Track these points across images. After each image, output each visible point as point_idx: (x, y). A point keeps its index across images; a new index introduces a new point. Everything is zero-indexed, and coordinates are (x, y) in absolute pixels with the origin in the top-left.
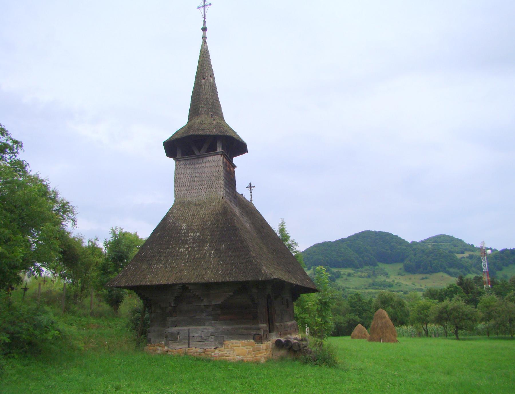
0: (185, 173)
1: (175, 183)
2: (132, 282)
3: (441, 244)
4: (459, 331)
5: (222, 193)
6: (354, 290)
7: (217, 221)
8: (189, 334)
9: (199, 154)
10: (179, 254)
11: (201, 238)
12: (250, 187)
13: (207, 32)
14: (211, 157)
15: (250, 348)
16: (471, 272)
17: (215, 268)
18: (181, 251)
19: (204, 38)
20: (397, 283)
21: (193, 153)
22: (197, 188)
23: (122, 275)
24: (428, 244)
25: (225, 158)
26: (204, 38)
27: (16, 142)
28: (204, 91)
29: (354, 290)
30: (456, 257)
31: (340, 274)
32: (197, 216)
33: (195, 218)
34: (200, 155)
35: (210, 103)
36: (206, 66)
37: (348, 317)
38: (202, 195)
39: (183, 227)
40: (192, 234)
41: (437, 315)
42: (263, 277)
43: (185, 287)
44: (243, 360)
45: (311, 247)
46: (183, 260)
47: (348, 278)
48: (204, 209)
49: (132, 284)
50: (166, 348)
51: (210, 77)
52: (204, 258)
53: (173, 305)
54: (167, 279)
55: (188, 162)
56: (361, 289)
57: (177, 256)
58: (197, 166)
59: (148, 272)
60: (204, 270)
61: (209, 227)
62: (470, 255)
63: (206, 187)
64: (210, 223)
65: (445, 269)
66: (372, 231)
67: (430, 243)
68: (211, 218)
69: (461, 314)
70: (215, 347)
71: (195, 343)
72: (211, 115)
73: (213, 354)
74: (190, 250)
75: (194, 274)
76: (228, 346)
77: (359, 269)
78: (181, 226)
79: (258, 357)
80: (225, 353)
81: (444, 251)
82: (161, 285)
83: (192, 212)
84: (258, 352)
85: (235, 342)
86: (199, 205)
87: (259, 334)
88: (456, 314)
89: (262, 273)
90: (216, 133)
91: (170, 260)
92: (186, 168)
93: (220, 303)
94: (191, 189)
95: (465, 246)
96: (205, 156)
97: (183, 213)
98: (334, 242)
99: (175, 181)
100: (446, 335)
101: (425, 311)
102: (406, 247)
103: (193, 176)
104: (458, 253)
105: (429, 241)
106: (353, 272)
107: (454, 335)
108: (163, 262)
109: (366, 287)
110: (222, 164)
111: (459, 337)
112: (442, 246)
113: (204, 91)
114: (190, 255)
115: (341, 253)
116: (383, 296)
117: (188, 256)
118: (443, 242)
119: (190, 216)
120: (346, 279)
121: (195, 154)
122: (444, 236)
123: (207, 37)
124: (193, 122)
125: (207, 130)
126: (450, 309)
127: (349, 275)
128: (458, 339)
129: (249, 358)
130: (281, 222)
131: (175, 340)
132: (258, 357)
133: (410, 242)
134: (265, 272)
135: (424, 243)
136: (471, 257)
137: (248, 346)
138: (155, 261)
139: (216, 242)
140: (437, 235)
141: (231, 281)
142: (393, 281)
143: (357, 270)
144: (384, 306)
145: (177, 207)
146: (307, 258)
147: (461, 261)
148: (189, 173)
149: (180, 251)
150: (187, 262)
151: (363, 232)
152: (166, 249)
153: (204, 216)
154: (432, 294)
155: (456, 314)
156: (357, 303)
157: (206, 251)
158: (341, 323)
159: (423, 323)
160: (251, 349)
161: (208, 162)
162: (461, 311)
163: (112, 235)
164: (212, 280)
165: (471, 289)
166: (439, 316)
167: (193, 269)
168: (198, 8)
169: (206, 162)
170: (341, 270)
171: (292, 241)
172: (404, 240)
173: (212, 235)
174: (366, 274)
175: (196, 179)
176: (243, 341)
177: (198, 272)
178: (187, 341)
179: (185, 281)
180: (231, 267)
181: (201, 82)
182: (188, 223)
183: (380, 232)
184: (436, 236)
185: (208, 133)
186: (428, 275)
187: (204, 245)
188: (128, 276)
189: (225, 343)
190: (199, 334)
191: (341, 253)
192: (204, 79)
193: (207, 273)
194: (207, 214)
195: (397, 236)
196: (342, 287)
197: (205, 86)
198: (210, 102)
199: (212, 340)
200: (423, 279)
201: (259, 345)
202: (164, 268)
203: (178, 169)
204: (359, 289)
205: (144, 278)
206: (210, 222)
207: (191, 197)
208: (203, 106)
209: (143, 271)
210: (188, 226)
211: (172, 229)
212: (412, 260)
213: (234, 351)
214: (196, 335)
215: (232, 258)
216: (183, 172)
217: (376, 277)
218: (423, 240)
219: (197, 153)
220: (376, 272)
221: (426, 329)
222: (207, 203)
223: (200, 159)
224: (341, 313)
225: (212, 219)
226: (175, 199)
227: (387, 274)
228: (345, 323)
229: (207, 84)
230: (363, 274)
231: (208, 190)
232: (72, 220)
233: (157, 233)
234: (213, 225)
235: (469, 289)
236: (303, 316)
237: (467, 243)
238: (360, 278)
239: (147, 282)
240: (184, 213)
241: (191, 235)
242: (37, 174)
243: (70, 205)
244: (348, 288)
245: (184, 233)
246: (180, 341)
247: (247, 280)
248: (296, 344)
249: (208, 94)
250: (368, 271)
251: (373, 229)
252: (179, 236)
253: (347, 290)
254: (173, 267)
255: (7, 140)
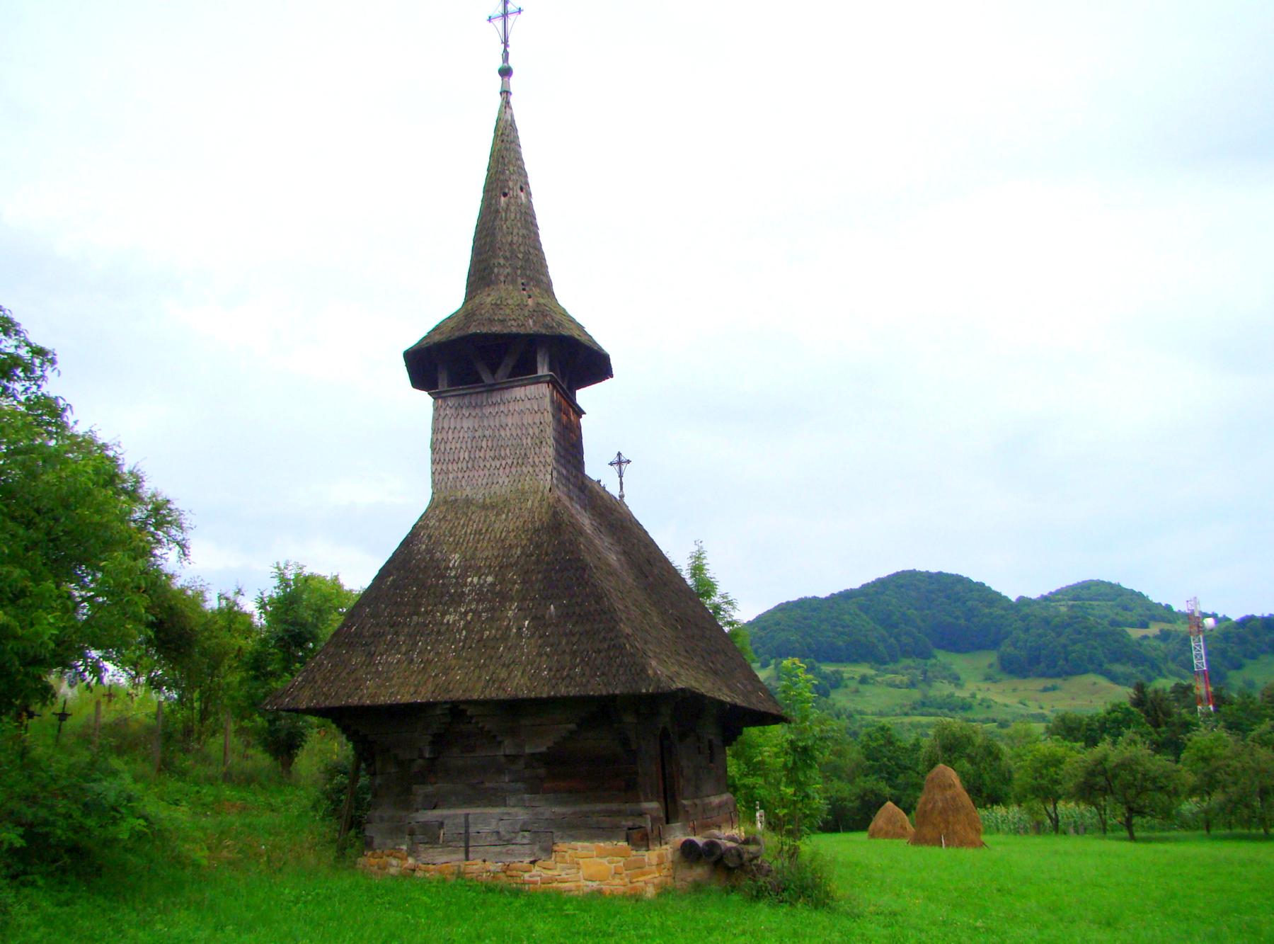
0: (458, 427)
1: (433, 453)
2: (326, 699)
3: (1091, 605)
4: (1136, 820)
5: (549, 477)
6: (876, 718)
7: (538, 546)
8: (467, 827)
9: (493, 382)
10: (443, 629)
11: (498, 588)
12: (620, 463)
13: (511, 79)
14: (523, 388)
15: (620, 862)
16: (1164, 671)
17: (532, 665)
18: (448, 621)
19: (506, 93)
20: (983, 700)
21: (478, 380)
22: (488, 466)
23: (303, 681)
24: (1059, 604)
25: (558, 391)
26: (506, 93)
27: (40, 352)
28: (505, 226)
29: (876, 718)
30: (1129, 636)
31: (842, 678)
32: (488, 536)
33: (483, 539)
34: (494, 384)
35: (520, 256)
36: (509, 162)
37: (862, 784)
38: (501, 482)
39: (453, 562)
40: (476, 580)
41: (1082, 780)
42: (650, 685)
43: (456, 710)
44: (600, 892)
45: (768, 611)
46: (452, 644)
47: (862, 688)
48: (504, 516)
49: (327, 703)
50: (411, 861)
51: (519, 191)
52: (505, 638)
53: (427, 755)
54: (412, 690)
55: (466, 401)
56: (893, 716)
57: (439, 633)
58: (487, 410)
59: (367, 674)
60: (504, 669)
61: (516, 563)
62: (1161, 631)
63: (510, 462)
64: (519, 552)
65: (1101, 665)
66: (920, 573)
67: (1062, 603)
68: (522, 539)
69: (1139, 776)
70: (532, 859)
71: (481, 849)
72: (523, 284)
73: (526, 876)
74: (469, 618)
75: (479, 677)
76: (563, 857)
77: (887, 666)
78: (447, 560)
79: (638, 884)
80: (556, 873)
81: (1099, 621)
82: (398, 705)
83: (475, 526)
84: (637, 870)
85: (582, 847)
86: (493, 507)
87: (640, 827)
88: (1128, 777)
89: (648, 676)
90: (535, 329)
91: (420, 644)
92: (460, 416)
93: (543, 749)
94: (473, 467)
95: (1149, 610)
96: (507, 385)
97: (452, 528)
98: (827, 599)
99: (434, 449)
100: (1103, 829)
101: (1052, 770)
102: (1003, 612)
103: (477, 435)
104: (1131, 626)
105: (1060, 597)
106: (872, 672)
107: (1124, 828)
108: (404, 649)
109: (906, 710)
110: (549, 405)
111: (1136, 834)
112: (1093, 609)
113: (505, 226)
114: (470, 632)
115: (843, 627)
116: (946, 732)
117: (464, 633)
118: (1096, 600)
119: (470, 534)
120: (857, 691)
121: (483, 382)
122: (1099, 583)
123: (512, 90)
124: (477, 300)
125: (513, 322)
126: (1114, 764)
127: (864, 680)
128: (1132, 838)
129: (616, 885)
130: (697, 548)
131: (433, 840)
132: (638, 884)
133: (1013, 598)
134: (656, 674)
135: (1048, 602)
136: (1165, 636)
137: (612, 855)
138: (383, 647)
139: (533, 599)
140: (1080, 581)
141: (571, 694)
142: (973, 696)
143: (883, 667)
144: (950, 756)
145: (437, 512)
146: (761, 638)
147: (1140, 645)
148: (469, 428)
149: (445, 621)
150: (463, 647)
151: (897, 575)
152: (410, 615)
153: (504, 534)
154: (1069, 729)
155: (1128, 777)
156: (884, 750)
157: (510, 621)
158: (844, 799)
159: (1045, 800)
160: (621, 864)
161: (515, 400)
162: (1140, 768)
163: (276, 582)
164: (524, 694)
165: (1164, 715)
166: (1085, 783)
167: (478, 667)
168: (490, 20)
169: (509, 402)
170: (843, 669)
171: (723, 597)
172: (998, 594)
173: (524, 582)
174: (905, 679)
175: (484, 444)
176: (602, 844)
177: (491, 672)
178: (463, 844)
179: (458, 695)
180: (571, 660)
181: (498, 203)
182: (466, 552)
183: (940, 573)
184: (1079, 583)
185: (514, 330)
186: (1058, 681)
187: (505, 607)
188: (316, 682)
189: (556, 848)
190: (493, 826)
191: (843, 627)
192: (505, 195)
193: (513, 675)
194: (513, 530)
195: (982, 585)
196: (845, 710)
197: (506, 213)
198: (520, 252)
199: (526, 841)
200: (1045, 690)
201: (640, 853)
202: (406, 663)
203: (441, 419)
204: (887, 715)
205: (357, 689)
206: (519, 548)
207: (474, 488)
208: (502, 261)
209: (355, 670)
210: (464, 558)
211: (425, 567)
212: (1019, 644)
213: (579, 869)
214: (486, 829)
215: (575, 640)
216: (452, 427)
217: (930, 686)
218: (1045, 593)
219: (487, 378)
220: (930, 674)
221: (1053, 815)
222: (511, 502)
223: (495, 394)
224: (844, 775)
225: (524, 542)
226: (433, 493)
227: (958, 678)
228: (853, 798)
229: (513, 208)
230: (898, 679)
231: (514, 470)
232: (178, 544)
233: (389, 577)
234: (527, 556)
235: (1161, 715)
236: (749, 781)
237: (1156, 601)
238: (891, 689)
239: (364, 699)
240: (456, 527)
241: (472, 581)
242: (91, 431)
243: (172, 507)
244: (861, 713)
245: (455, 577)
246: (446, 844)
247: (611, 692)
248: (733, 851)
249: (515, 231)
250: (910, 671)
251: (922, 567)
252: (443, 584)
253: (858, 717)
254: (429, 662)
255: (16, 347)
